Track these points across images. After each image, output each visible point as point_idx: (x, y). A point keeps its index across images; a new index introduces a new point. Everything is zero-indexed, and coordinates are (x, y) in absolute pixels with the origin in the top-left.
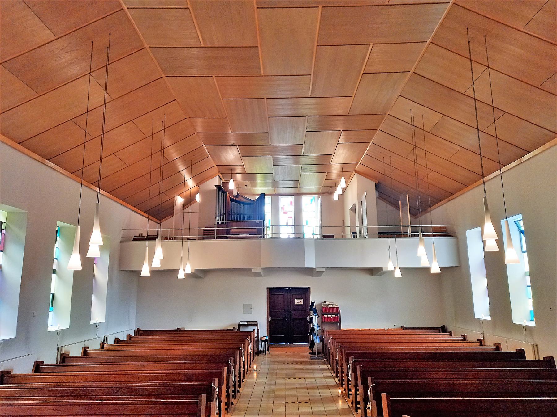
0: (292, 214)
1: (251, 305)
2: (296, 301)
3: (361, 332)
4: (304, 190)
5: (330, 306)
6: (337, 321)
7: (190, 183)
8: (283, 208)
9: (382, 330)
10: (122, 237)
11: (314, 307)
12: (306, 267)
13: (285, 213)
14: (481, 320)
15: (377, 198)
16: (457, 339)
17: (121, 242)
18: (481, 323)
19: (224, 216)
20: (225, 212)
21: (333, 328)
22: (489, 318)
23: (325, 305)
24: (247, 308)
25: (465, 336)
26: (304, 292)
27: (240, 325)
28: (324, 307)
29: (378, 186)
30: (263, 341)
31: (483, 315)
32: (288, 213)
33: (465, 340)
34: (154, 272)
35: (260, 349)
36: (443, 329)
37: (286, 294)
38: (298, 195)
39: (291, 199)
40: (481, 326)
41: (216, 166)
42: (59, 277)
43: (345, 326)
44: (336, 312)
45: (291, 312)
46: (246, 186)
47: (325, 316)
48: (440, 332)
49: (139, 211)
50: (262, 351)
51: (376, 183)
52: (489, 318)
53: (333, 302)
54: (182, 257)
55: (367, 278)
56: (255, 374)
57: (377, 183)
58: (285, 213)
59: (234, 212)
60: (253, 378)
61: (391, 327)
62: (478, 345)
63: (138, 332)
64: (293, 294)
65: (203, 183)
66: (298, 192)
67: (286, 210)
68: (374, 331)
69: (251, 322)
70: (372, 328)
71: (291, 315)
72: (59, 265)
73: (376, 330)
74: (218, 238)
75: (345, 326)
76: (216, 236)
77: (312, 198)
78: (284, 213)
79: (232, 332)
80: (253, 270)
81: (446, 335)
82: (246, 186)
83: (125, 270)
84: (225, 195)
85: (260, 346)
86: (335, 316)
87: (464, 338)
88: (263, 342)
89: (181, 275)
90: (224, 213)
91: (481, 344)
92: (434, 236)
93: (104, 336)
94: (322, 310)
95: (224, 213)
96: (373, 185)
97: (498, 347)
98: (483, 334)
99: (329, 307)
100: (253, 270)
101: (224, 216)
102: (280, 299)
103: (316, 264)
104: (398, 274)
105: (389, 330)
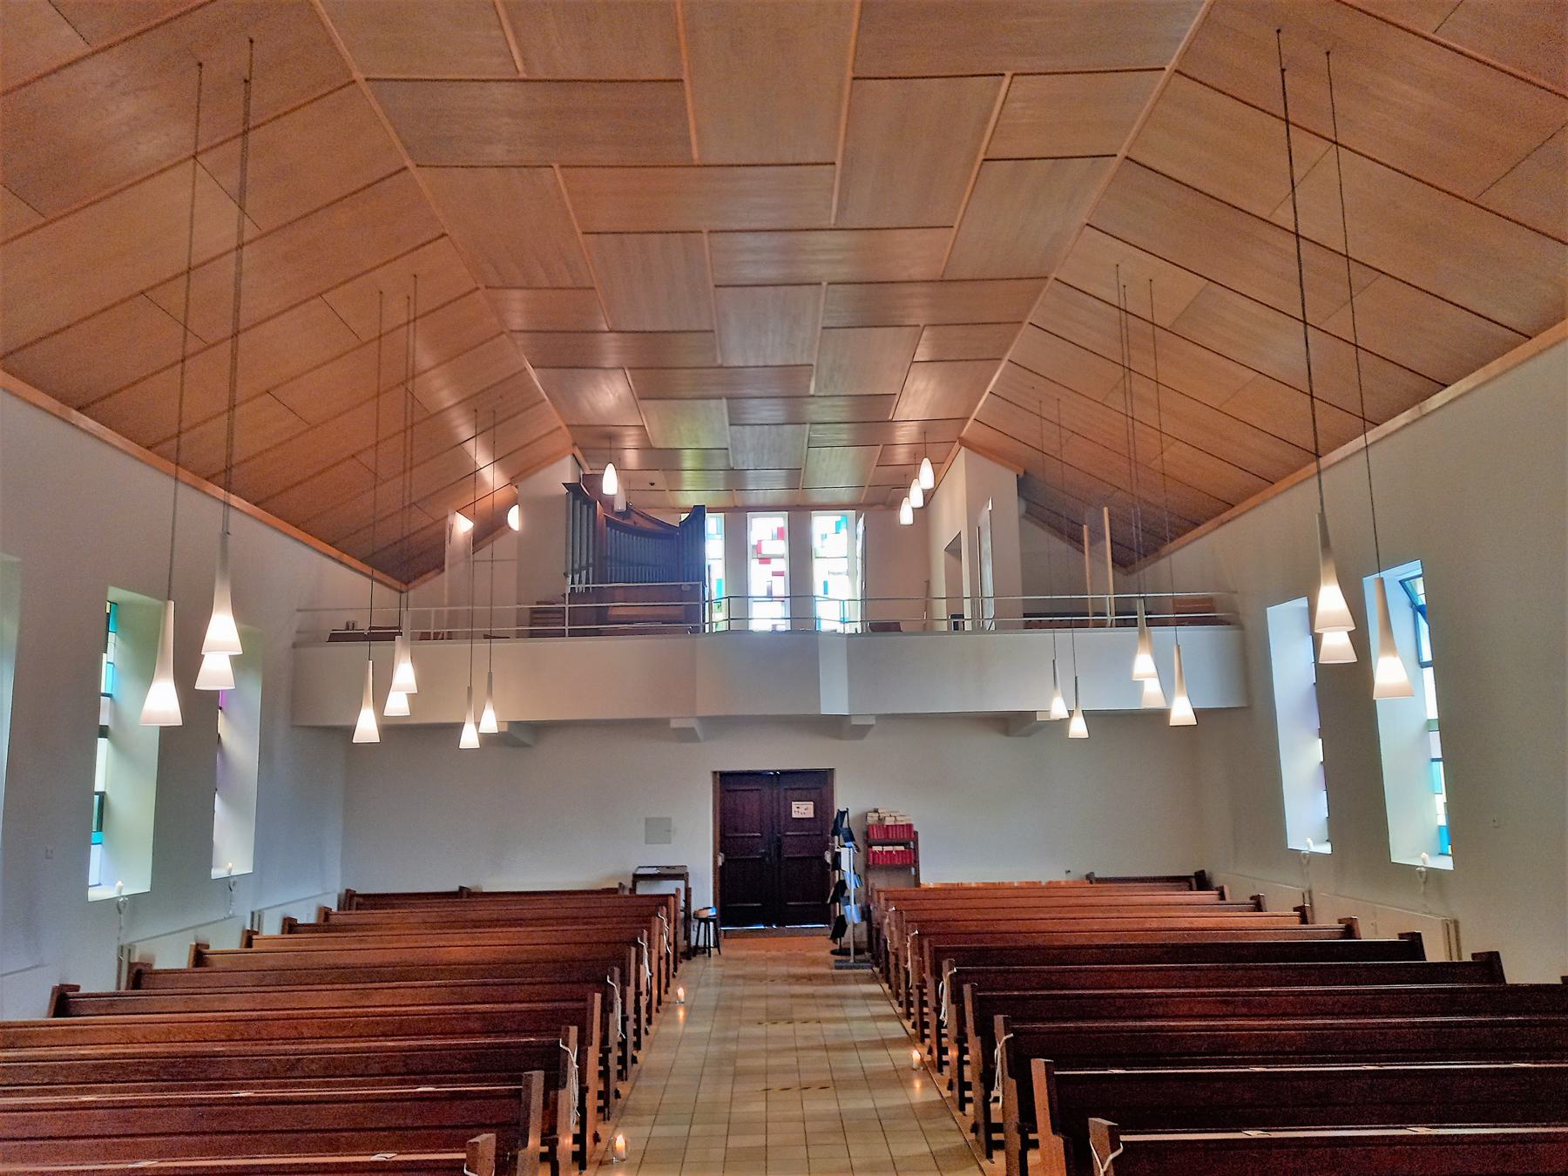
0: (782, 565)
1: (670, 819)
2: (794, 808)
3: (972, 893)
4: (817, 497)
5: (889, 821)
6: (909, 861)
7: (492, 476)
8: (758, 548)
9: (1034, 886)
10: (298, 632)
11: (845, 825)
12: (825, 711)
13: (765, 560)
14: (1305, 854)
15: (1022, 517)
16: (1238, 906)
17: (295, 646)
18: (1305, 862)
19: (591, 569)
20: (594, 559)
21: (898, 883)
22: (1326, 849)
23: (877, 819)
24: (659, 830)
25: (1262, 899)
26: (817, 782)
27: (637, 878)
28: (872, 826)
29: (1025, 485)
30: (701, 920)
31: (1309, 840)
32: (773, 561)
33: (1260, 910)
34: (390, 729)
35: (693, 943)
36: (1201, 881)
37: (766, 791)
38: (799, 511)
39: (779, 521)
40: (1305, 871)
41: (565, 428)
42: (117, 746)
43: (932, 875)
44: (906, 837)
45: (779, 840)
46: (652, 484)
47: (875, 848)
48: (1191, 890)
49: (346, 558)
50: (700, 948)
51: (1017, 475)
52: (1326, 849)
53: (896, 810)
54: (470, 689)
55: (991, 743)
56: (681, 1013)
57: (1021, 475)
58: (765, 560)
59: (623, 558)
60: (675, 1022)
61: (1058, 876)
62: (1295, 922)
63: (350, 900)
64: (786, 789)
65: (529, 475)
66: (799, 501)
67: (766, 551)
68: (1011, 888)
69: (668, 867)
70: (1006, 880)
71: (779, 847)
72: (116, 712)
73: (1016, 885)
74: (573, 633)
75: (932, 875)
76: (567, 628)
77: (839, 518)
78: (760, 563)
79: (615, 895)
80: (674, 724)
81: (1209, 896)
82: (652, 484)
83: (309, 727)
84: (591, 511)
85: (694, 934)
86: (902, 848)
87: (1257, 904)
88: (703, 924)
89: (469, 739)
90: (591, 561)
91: (1304, 920)
92: (1180, 622)
93: (253, 913)
94: (867, 834)
95: (591, 561)
96: (1007, 480)
97: (1349, 929)
98: (1310, 892)
99: (887, 823)
100: (674, 724)
101: (591, 569)
102: (751, 802)
103: (850, 705)
104: (1078, 728)
105: (1051, 886)
